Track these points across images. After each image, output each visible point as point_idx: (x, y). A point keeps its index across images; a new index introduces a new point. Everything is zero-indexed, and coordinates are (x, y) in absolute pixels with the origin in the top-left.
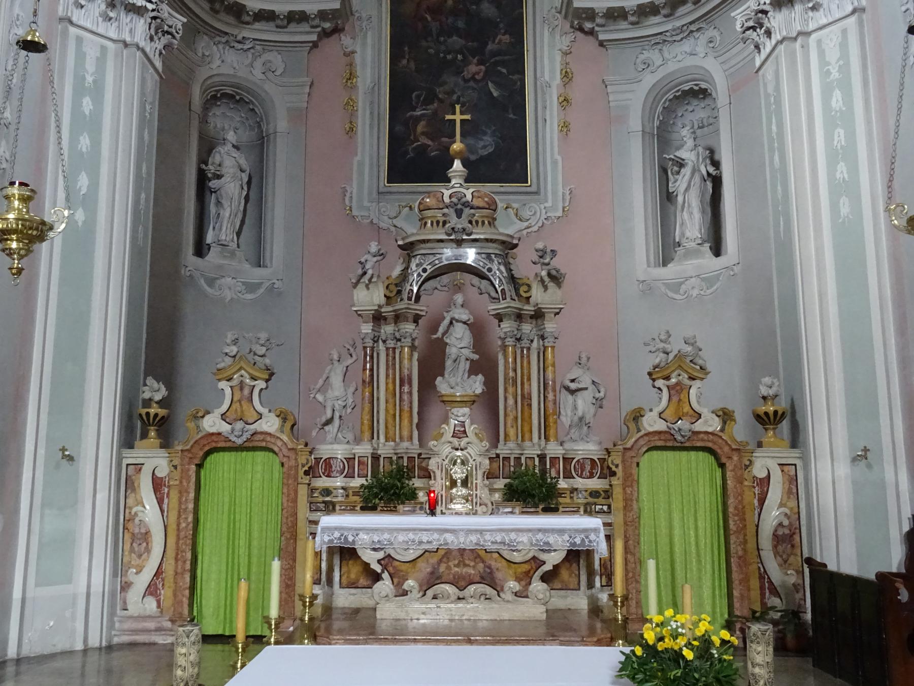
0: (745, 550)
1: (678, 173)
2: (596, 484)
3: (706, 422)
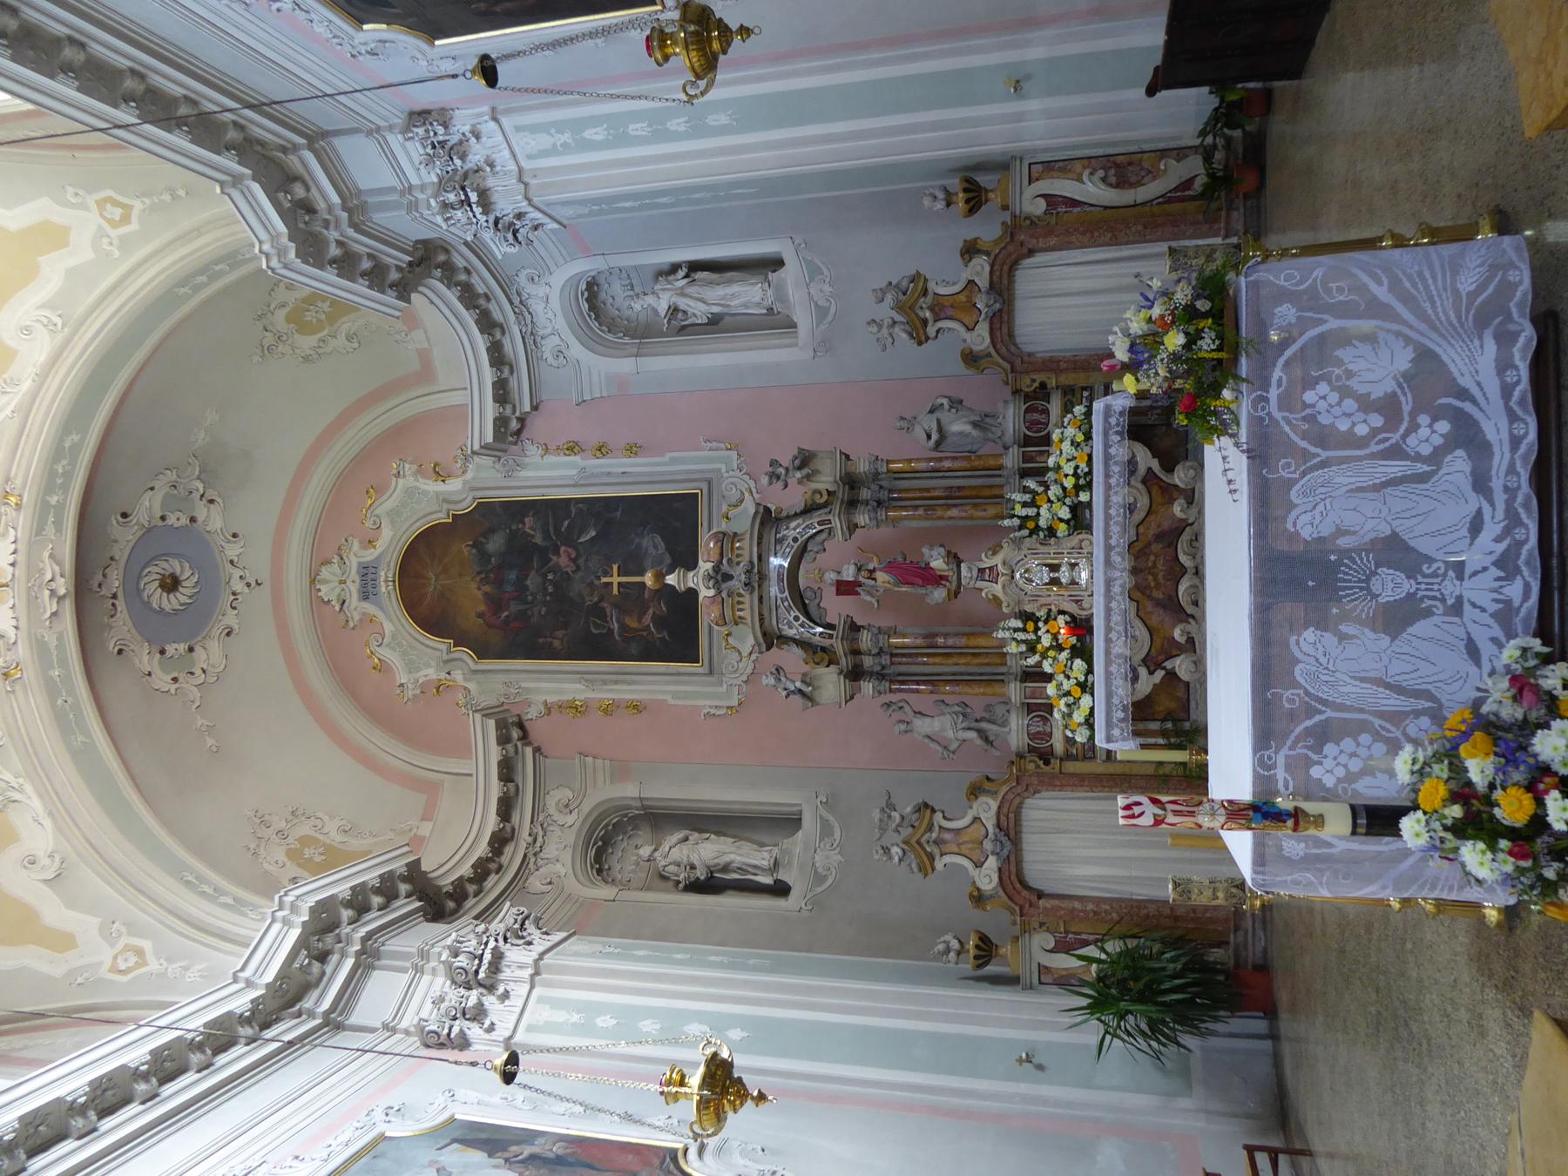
1: (685, 312)
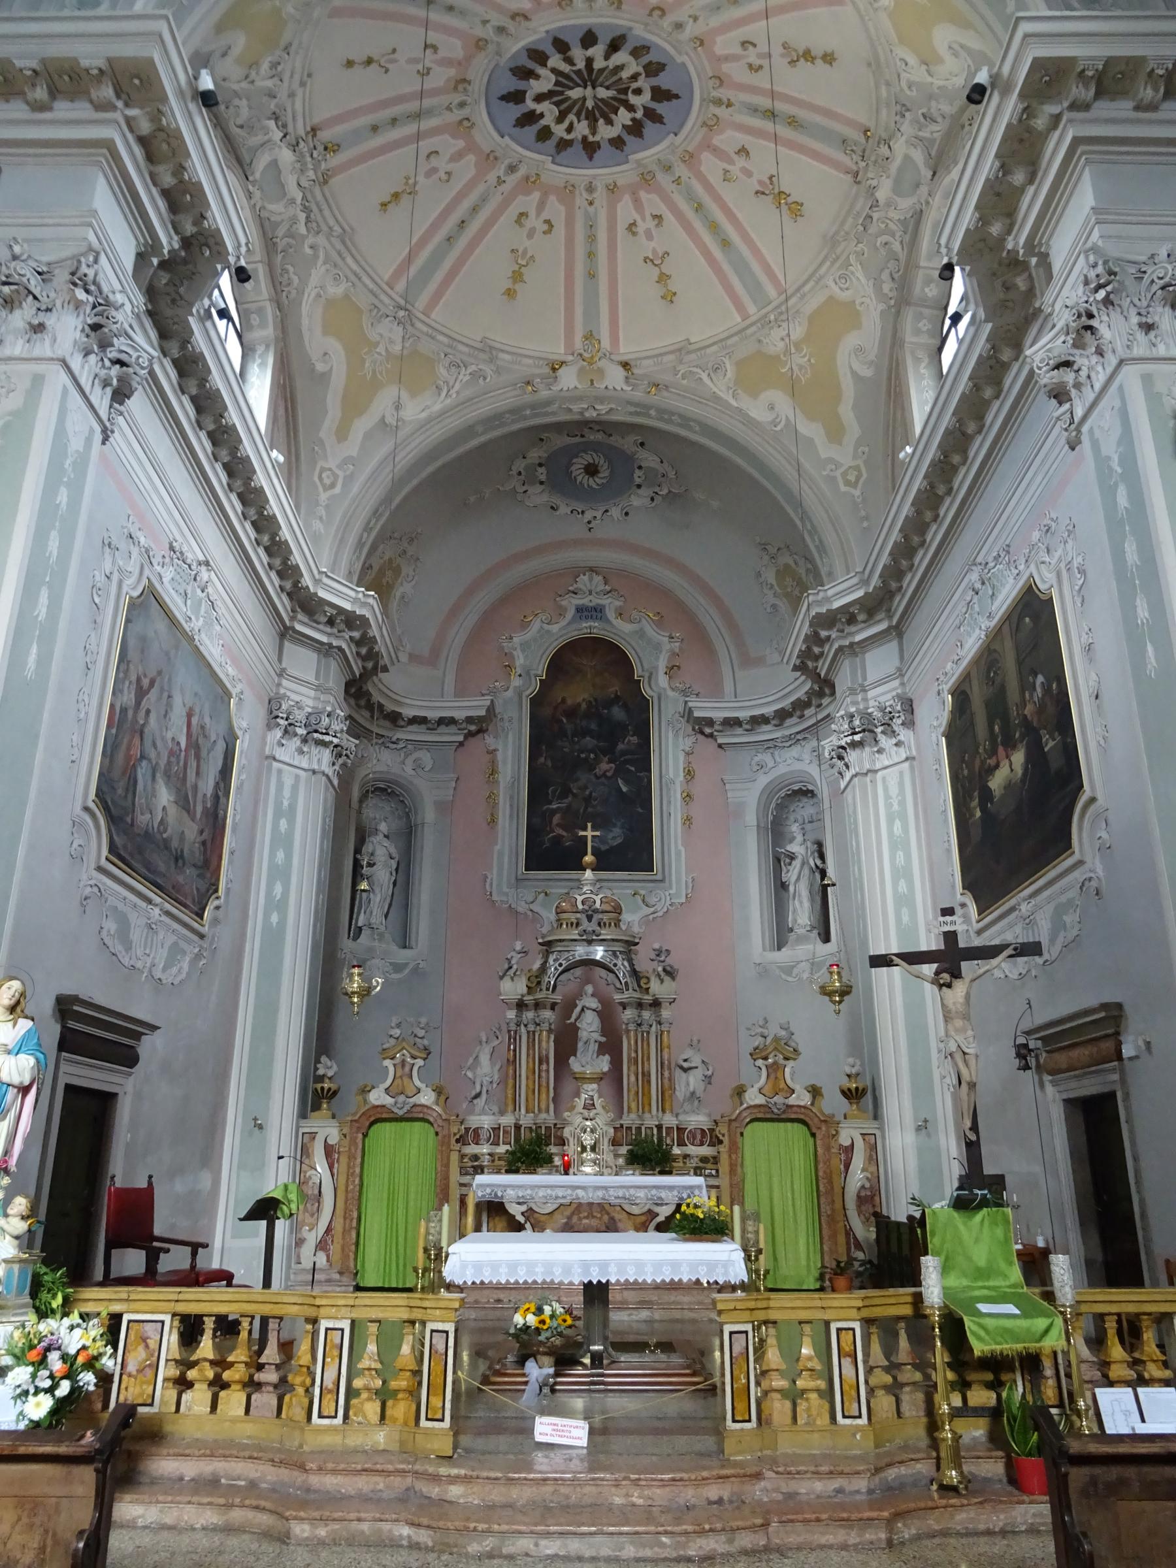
0: (833, 1210)
2: (706, 1151)
3: (798, 1098)
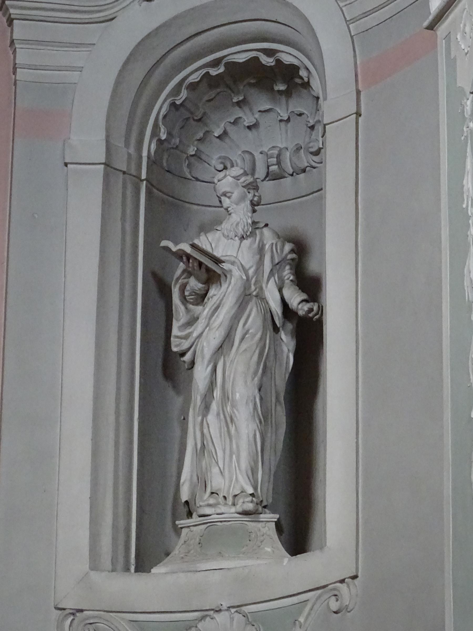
1: (201, 298)
